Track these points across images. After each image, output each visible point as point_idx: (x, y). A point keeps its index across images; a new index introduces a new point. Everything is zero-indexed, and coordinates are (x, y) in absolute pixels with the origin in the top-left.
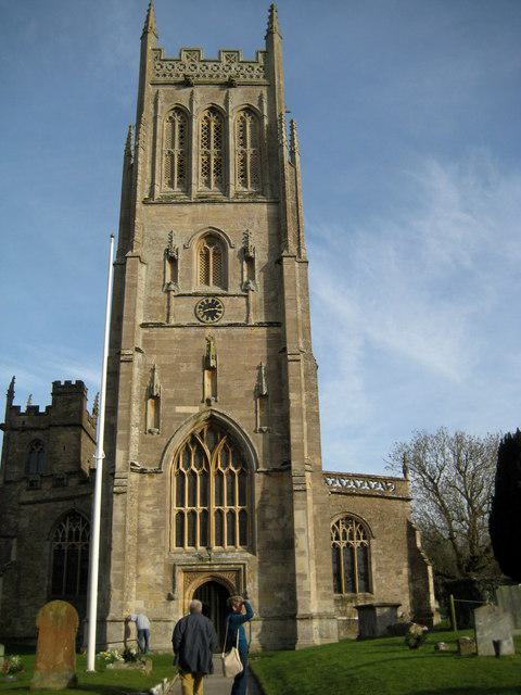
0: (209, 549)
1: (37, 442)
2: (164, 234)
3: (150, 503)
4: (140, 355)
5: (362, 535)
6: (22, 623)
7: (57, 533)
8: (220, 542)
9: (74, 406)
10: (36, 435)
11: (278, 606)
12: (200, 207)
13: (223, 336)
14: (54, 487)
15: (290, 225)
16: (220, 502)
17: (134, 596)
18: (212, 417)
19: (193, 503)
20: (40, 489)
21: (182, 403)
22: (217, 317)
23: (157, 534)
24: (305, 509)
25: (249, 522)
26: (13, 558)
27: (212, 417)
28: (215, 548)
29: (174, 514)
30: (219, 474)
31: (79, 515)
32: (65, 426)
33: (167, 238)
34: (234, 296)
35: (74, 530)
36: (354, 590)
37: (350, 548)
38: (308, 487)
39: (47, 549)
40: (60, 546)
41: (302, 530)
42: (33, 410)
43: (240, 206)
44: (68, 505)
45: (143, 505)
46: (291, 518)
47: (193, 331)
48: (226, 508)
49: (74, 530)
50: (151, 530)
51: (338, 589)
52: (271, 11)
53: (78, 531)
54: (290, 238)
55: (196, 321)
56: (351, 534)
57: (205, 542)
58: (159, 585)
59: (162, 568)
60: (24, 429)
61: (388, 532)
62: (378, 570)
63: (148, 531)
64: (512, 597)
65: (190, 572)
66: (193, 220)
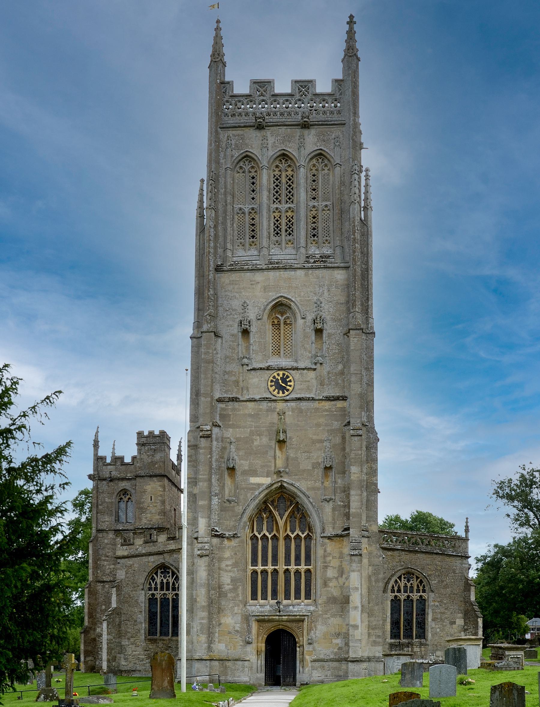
1: (125, 492)
3: (229, 563)
5: (421, 588)
6: (125, 659)
7: (150, 584)
8: (287, 596)
9: (158, 457)
10: (124, 485)
11: (336, 650)
12: (272, 274)
13: (293, 410)
14: (146, 542)
18: (282, 487)
20: (133, 544)
21: (254, 473)
23: (235, 589)
26: (114, 605)
27: (282, 487)
29: (249, 573)
30: (287, 537)
31: (169, 568)
32: (151, 476)
34: (303, 369)
35: (165, 581)
36: (411, 637)
38: (364, 552)
39: (142, 597)
40: (153, 595)
42: (118, 460)
43: (310, 271)
47: (264, 405)
49: (165, 581)
50: (230, 587)
51: (395, 635)
53: (168, 583)
55: (269, 396)
56: (412, 587)
57: (275, 595)
58: (237, 631)
59: (240, 618)
60: (112, 480)
61: (446, 586)
64: (455, 654)
65: (261, 621)
66: (265, 289)
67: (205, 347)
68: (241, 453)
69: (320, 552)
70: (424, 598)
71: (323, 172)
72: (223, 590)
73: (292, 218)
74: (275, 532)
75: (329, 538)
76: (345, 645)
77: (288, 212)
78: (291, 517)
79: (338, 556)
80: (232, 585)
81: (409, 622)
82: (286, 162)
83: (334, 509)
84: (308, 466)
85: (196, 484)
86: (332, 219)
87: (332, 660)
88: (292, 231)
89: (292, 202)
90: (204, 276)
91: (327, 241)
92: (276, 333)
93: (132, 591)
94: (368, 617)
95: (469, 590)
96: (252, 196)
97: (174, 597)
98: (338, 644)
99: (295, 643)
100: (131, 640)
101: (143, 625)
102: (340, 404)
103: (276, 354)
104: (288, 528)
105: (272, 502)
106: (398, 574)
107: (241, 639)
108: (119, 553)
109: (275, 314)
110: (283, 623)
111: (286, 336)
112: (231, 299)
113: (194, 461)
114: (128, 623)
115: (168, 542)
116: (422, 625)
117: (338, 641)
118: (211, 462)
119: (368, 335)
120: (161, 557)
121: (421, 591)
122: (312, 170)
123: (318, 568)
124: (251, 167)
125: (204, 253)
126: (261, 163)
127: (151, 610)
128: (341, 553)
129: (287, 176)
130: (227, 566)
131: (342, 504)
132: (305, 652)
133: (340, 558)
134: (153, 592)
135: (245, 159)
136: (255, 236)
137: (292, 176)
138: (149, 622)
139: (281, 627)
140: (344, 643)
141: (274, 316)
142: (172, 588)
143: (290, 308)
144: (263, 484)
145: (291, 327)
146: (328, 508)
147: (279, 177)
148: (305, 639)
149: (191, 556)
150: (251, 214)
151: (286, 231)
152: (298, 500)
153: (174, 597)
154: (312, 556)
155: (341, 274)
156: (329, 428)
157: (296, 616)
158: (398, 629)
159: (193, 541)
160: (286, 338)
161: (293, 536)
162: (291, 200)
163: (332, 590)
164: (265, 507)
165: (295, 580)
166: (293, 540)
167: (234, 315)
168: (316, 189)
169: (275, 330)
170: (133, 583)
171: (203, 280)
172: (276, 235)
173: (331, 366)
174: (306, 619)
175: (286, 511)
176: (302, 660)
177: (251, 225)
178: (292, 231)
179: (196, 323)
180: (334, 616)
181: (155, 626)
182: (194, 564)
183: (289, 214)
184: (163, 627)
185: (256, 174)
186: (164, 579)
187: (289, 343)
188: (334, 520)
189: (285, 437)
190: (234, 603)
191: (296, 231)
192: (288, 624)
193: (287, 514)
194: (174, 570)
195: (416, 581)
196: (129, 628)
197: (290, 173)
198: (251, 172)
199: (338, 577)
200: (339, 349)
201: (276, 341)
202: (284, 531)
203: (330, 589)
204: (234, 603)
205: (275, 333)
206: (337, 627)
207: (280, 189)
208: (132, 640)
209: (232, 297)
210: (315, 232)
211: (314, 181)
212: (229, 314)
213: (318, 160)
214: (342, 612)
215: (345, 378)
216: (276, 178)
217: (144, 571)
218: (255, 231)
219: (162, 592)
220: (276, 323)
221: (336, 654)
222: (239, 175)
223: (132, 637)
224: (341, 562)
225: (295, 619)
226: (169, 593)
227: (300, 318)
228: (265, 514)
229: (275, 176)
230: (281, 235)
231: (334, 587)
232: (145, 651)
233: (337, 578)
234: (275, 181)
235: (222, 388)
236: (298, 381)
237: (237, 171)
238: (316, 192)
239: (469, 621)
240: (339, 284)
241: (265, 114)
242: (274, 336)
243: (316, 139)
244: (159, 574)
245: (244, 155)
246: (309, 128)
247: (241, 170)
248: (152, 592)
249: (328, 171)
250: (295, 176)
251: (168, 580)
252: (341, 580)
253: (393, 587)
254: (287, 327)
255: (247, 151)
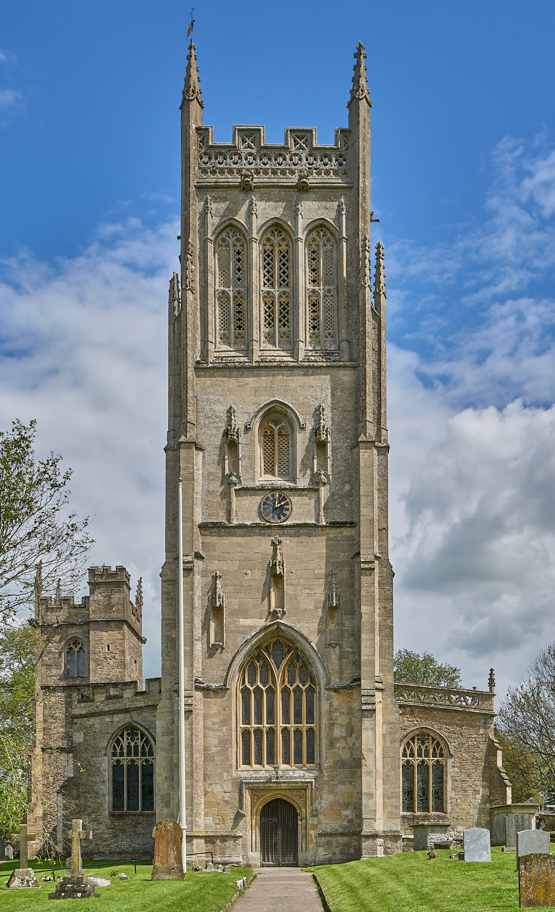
0: (276, 769)
2: (221, 409)
3: (216, 720)
4: (200, 562)
5: (438, 752)
7: (114, 748)
11: (345, 823)
15: (370, 399)
16: (286, 720)
17: (203, 813)
19: (259, 720)
21: (245, 614)
22: (284, 515)
24: (374, 729)
25: (316, 748)
28: (283, 766)
31: (138, 729)
33: (224, 416)
35: (132, 744)
37: (423, 766)
40: (118, 761)
41: (370, 750)
44: (120, 719)
45: (209, 723)
46: (359, 737)
48: (292, 726)
49: (132, 744)
51: (409, 807)
52: (357, 56)
53: (136, 747)
54: (369, 416)
56: (427, 751)
57: (272, 760)
62: (453, 789)
63: (214, 750)
67: (184, 462)
68: (231, 589)
69: (325, 707)
70: (441, 763)
71: (325, 248)
72: (210, 752)
73: (287, 305)
74: (270, 683)
75: (336, 690)
76: (356, 816)
77: (282, 297)
78: (289, 666)
79: (346, 712)
80: (220, 747)
81: (424, 792)
82: (279, 235)
83: (341, 657)
84: (309, 606)
85: (175, 626)
86: (336, 307)
87: (342, 834)
88: (287, 321)
89: (287, 285)
90: (180, 374)
91: (329, 334)
92: (269, 446)
93: (92, 757)
94: (383, 783)
95: (495, 755)
96: (237, 276)
97: (144, 763)
98: (348, 816)
99: (297, 815)
100: (92, 817)
101: (107, 798)
102: (347, 532)
103: (269, 471)
104: (287, 679)
105: (267, 649)
106: (411, 736)
107: (231, 811)
108: (76, 712)
109: (268, 423)
110: (281, 792)
111: (281, 450)
112: (214, 404)
113: (172, 599)
114: (88, 796)
115: (134, 698)
116: (440, 795)
117: (347, 813)
118: (193, 600)
119: (380, 449)
120: (128, 715)
121: (438, 755)
122: (311, 245)
123: (323, 727)
124: (236, 239)
125: (180, 346)
126: (249, 235)
127: (115, 780)
128: (350, 709)
129: (281, 252)
130: (214, 723)
131: (350, 650)
132: (308, 826)
133: (348, 714)
134: (118, 758)
135: (229, 228)
136: (241, 327)
137: (287, 252)
138: (113, 794)
139: (279, 797)
140: (354, 815)
141: (267, 425)
142: (142, 752)
143: (285, 415)
144: (256, 627)
145: (286, 439)
146: (334, 655)
147: (270, 254)
148: (309, 810)
149: (170, 712)
150: (236, 299)
151: (280, 321)
152: (298, 645)
153: (144, 763)
154: (315, 712)
155: (347, 375)
156: (335, 560)
157: (297, 782)
158: (412, 799)
159: (172, 695)
160: (281, 452)
161: (291, 688)
162: (286, 282)
163: (340, 752)
164: (258, 654)
165: (295, 741)
166: (292, 694)
167: (217, 423)
168: (316, 270)
169: (267, 442)
170: (93, 748)
171: (180, 379)
172: (267, 326)
173: (337, 486)
174: (309, 787)
175: (283, 659)
176: (306, 836)
177: (237, 313)
178: (287, 321)
179: (172, 432)
180: (342, 782)
181: (120, 798)
182: (174, 722)
183: (284, 299)
184: (130, 799)
185: (242, 248)
186: (131, 742)
187: (285, 458)
188: (342, 669)
189: (282, 570)
190: (222, 768)
191: (292, 321)
192: (288, 793)
193: (284, 662)
194: (144, 730)
195: (432, 743)
196: (89, 801)
197: (284, 248)
198: (236, 246)
199: (347, 736)
200: (345, 466)
201: (269, 456)
202: (282, 682)
203: (337, 750)
204: (222, 768)
205: (267, 446)
206: (346, 796)
207: (272, 268)
208: (93, 816)
209: (215, 401)
210: (315, 323)
211: (314, 259)
212: (212, 421)
213: (319, 233)
214: (352, 777)
215: (352, 500)
216: (266, 254)
217: (107, 733)
218: (241, 320)
219: (130, 758)
220: (269, 434)
221: (345, 827)
222: (222, 250)
223: (92, 812)
224: (350, 719)
225: (296, 786)
226: (138, 759)
227: (298, 428)
228: (258, 662)
229: (265, 252)
230: (273, 326)
231: (343, 748)
232: (110, 828)
233: (345, 738)
234: (266, 258)
235: (204, 511)
236: (297, 504)
237: (219, 244)
238: (316, 274)
239: (496, 790)
240: (345, 387)
241: (253, 171)
242: (267, 450)
243: (317, 205)
244: (125, 736)
245: (227, 223)
246: (308, 192)
247: (223, 243)
248: (117, 758)
249: (331, 247)
250: (291, 252)
251: (136, 743)
252: (350, 741)
253: (405, 750)
254: (282, 439)
255: (231, 219)
